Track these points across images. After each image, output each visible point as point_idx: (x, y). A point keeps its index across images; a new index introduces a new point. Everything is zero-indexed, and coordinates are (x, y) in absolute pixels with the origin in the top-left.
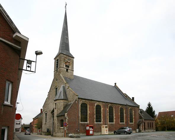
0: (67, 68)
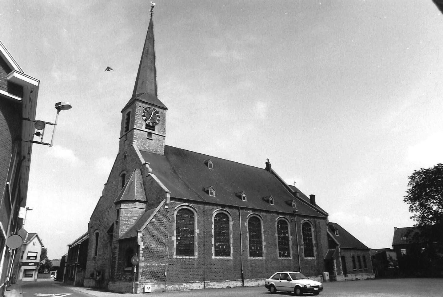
0: (148, 130)
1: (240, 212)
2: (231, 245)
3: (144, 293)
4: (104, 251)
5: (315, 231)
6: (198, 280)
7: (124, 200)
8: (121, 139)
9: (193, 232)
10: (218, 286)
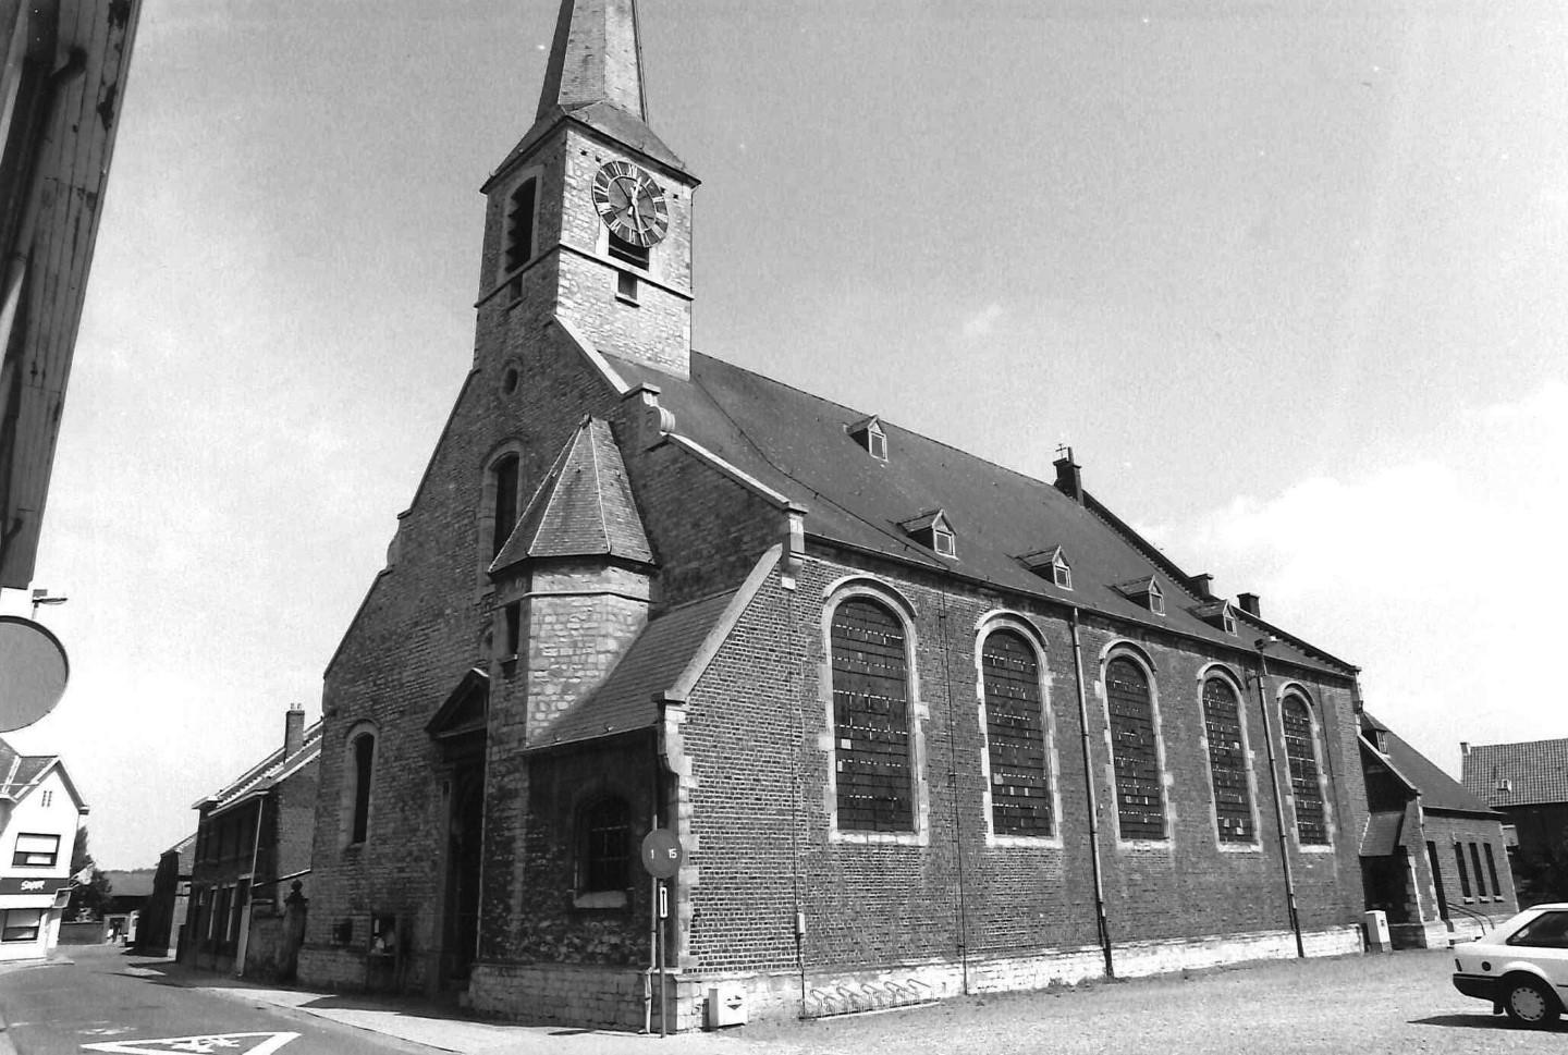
1: (1076, 630)
2: (1054, 785)
3: (709, 1026)
4: (406, 819)
5: (1324, 733)
6: (937, 954)
7: (549, 553)
8: (482, 307)
9: (901, 715)
10: (1018, 980)
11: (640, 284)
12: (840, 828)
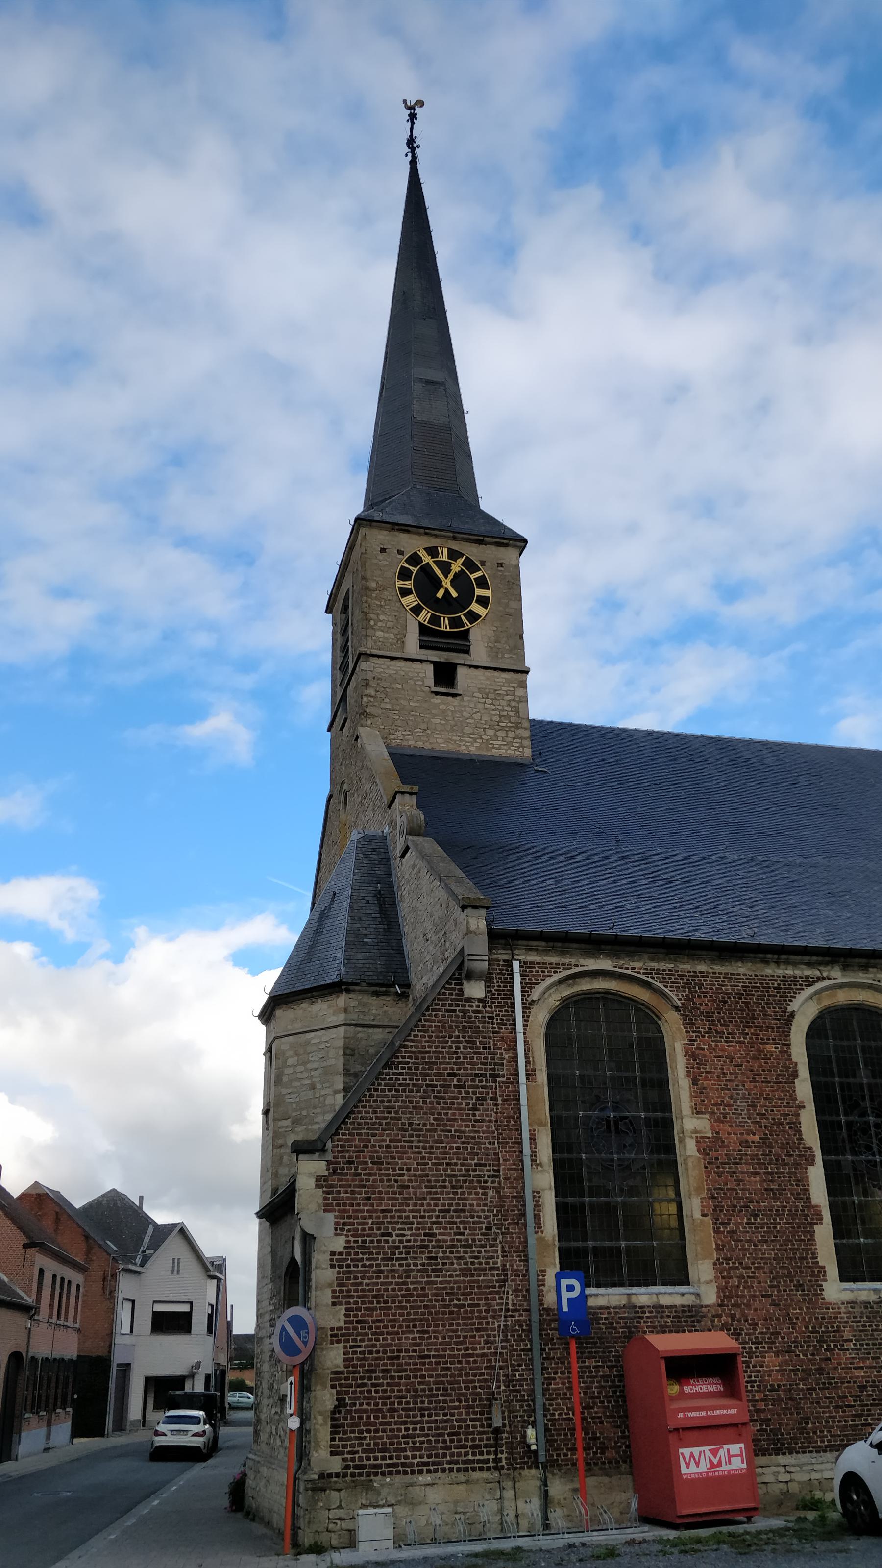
8: (333, 729)
11: (461, 672)
12: (843, 1278)
